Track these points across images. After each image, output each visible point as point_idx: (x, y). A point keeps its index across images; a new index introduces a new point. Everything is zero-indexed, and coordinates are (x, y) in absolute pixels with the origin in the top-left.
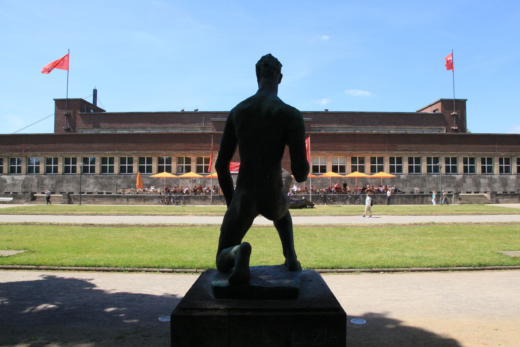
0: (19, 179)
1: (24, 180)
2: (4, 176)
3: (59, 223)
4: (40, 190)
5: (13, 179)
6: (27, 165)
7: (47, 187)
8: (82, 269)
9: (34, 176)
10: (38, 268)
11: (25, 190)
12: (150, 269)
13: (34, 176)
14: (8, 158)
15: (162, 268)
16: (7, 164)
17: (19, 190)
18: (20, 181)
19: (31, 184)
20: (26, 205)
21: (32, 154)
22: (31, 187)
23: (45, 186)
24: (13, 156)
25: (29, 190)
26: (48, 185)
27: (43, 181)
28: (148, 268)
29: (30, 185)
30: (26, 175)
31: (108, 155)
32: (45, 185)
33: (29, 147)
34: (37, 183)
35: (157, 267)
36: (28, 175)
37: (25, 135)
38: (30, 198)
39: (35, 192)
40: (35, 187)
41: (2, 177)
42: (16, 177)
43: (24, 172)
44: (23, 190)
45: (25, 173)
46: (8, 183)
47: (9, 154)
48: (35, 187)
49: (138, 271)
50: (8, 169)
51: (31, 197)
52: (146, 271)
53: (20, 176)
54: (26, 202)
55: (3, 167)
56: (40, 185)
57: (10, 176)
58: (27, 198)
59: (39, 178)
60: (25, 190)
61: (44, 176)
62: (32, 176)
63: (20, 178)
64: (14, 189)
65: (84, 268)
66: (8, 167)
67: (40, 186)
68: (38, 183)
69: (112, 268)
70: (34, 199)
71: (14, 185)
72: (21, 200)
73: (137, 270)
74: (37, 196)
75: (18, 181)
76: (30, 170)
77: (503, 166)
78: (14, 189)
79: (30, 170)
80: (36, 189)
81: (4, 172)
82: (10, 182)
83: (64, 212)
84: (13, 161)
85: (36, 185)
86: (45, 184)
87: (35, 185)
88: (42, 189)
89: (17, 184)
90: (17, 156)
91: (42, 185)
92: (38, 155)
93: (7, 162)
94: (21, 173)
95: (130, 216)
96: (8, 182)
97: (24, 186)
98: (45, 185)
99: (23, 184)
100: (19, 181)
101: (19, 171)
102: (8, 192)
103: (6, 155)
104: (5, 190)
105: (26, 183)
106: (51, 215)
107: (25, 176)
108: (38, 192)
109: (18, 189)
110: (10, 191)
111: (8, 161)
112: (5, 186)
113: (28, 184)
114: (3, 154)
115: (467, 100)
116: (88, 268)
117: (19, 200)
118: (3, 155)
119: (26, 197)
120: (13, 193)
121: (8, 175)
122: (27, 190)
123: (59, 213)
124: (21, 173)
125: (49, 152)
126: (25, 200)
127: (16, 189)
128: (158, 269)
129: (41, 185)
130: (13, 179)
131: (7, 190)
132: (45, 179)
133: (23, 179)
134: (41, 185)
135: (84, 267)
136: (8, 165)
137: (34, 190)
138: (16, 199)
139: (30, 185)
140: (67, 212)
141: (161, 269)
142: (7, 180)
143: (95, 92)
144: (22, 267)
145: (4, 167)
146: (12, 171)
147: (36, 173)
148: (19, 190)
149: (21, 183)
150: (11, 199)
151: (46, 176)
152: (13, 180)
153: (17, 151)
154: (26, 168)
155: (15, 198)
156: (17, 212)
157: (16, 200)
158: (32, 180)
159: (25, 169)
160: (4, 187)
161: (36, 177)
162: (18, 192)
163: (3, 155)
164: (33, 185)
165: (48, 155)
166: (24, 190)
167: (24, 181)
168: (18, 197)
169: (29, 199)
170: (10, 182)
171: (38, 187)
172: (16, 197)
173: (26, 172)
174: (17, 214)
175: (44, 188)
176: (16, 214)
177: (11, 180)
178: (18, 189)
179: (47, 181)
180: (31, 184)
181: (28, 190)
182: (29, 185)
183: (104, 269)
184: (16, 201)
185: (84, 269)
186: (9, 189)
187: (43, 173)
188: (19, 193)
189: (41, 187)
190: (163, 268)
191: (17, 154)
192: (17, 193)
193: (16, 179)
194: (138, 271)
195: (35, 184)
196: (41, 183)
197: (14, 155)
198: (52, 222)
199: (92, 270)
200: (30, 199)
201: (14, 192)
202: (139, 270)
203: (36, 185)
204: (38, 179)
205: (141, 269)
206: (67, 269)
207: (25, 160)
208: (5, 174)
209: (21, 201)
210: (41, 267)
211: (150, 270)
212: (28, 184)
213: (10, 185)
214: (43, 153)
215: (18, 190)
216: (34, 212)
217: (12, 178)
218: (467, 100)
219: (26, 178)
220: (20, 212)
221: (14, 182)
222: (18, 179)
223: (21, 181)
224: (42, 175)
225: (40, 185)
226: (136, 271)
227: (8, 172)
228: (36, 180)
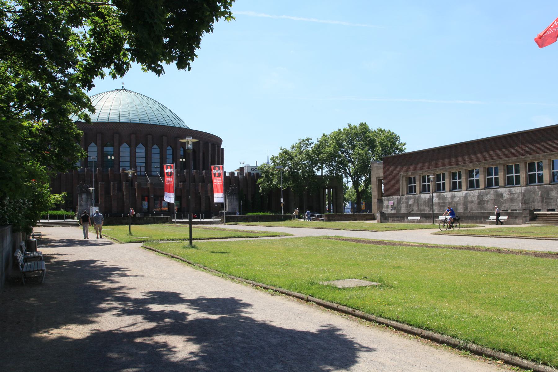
0: (518, 192)
1: (523, 193)
2: (500, 189)
3: (510, 250)
4: (545, 206)
5: (511, 193)
6: (526, 172)
7: (554, 201)
8: (403, 328)
9: (536, 187)
10: (354, 312)
11: (526, 206)
12: (517, 359)
13: (536, 186)
14: (504, 165)
15: (543, 364)
16: (502, 173)
17: (518, 206)
18: (519, 194)
19: (534, 198)
20: (523, 226)
21: (532, 157)
22: (533, 202)
23: (552, 201)
24: (509, 163)
25: (531, 206)
26: (555, 198)
27: (548, 194)
28: (512, 354)
29: (531, 200)
30: (526, 186)
31: (471, 167)
32: (551, 199)
33: (528, 148)
34: (541, 196)
35: (533, 357)
36: (528, 186)
37: (521, 133)
38: (528, 217)
39: (539, 208)
40: (538, 202)
41: (498, 191)
42: (513, 190)
43: (523, 182)
44: (523, 206)
45: (525, 183)
46: (505, 198)
47: (504, 160)
48: (538, 202)
49: (490, 356)
50: (505, 180)
51: (530, 215)
52: (507, 362)
53: (519, 188)
54: (524, 222)
55: (498, 177)
56: (545, 198)
57: (506, 189)
58: (525, 217)
59: (543, 190)
60: (526, 206)
61: (550, 186)
62: (534, 187)
63: (519, 190)
64: (512, 205)
65: (406, 327)
66: (504, 177)
67: (545, 201)
68: (541, 196)
69: (445, 338)
70: (533, 218)
71: (512, 200)
72: (517, 220)
73: (489, 353)
74: (538, 214)
75: (516, 195)
76: (531, 180)
77: (515, 173)
78: (512, 205)
79: (531, 180)
80: (540, 204)
81: (499, 185)
82: (508, 196)
83: (551, 236)
84: (509, 170)
85: (539, 199)
86: (552, 197)
87: (538, 199)
88: (548, 205)
89: (515, 200)
90: (513, 162)
91: (548, 198)
92: (540, 158)
93: (502, 170)
94: (519, 184)
95: (456, 236)
96: (505, 196)
97: (525, 201)
98: (551, 199)
99: (523, 198)
100: (518, 195)
101: (518, 182)
102: (505, 209)
103: (501, 162)
104: (502, 207)
105: (527, 197)
106: (531, 239)
107: (525, 187)
108: (543, 209)
109: (518, 205)
110: (507, 208)
111: (504, 170)
112: (502, 201)
113: (529, 198)
114: (497, 161)
116: (411, 327)
117: (515, 220)
118: (498, 162)
119: (523, 216)
120: (512, 210)
121: (504, 188)
122: (528, 206)
123: (543, 236)
124: (519, 184)
125: (554, 152)
126: (522, 219)
127: (514, 205)
128: (533, 363)
129: (546, 199)
130: (511, 193)
131: (505, 206)
132: (551, 190)
133: (523, 191)
134: (546, 199)
135: (406, 326)
136: (504, 174)
137: (537, 206)
138: (512, 219)
139: (531, 200)
140: (554, 236)
141: (540, 366)
142: (504, 195)
143: (256, 161)
144: (341, 307)
145: (499, 178)
146: (509, 182)
147: (539, 182)
148: (518, 206)
149: (521, 197)
150: (419, 218)
151: (552, 185)
152: (511, 194)
153: (513, 155)
154: (526, 177)
155: (510, 218)
156: (488, 234)
157: (511, 220)
158: (534, 192)
159: (524, 179)
160: (500, 203)
161: (539, 188)
162: (518, 209)
163: (498, 162)
164: (536, 199)
165: (553, 156)
166: (525, 206)
167: (524, 194)
168: (514, 216)
169: (527, 218)
170: (508, 196)
171: (542, 202)
172: (512, 216)
173: (526, 182)
174: (488, 237)
175: (551, 202)
176: (487, 236)
177: (509, 194)
178: (518, 205)
179: (554, 192)
180: (534, 198)
181: (529, 207)
182: (531, 199)
183: (433, 336)
184: (512, 220)
185: (406, 328)
186: (506, 206)
187: (548, 182)
188: (519, 210)
189: (546, 202)
190: (547, 365)
191: (513, 159)
192: (516, 210)
193: (514, 192)
194: (490, 356)
195: (538, 198)
196: (546, 196)
197: (510, 161)
198: (471, 244)
199: (415, 334)
200: (528, 218)
201: (513, 209)
202: (492, 354)
203: (539, 199)
204: (542, 191)
205: (497, 355)
206: (385, 322)
207: (524, 166)
208: (501, 187)
209: (517, 221)
210: (357, 311)
211: (516, 362)
212: (529, 198)
213: (507, 200)
214: (546, 154)
215: (517, 207)
216: (509, 235)
217: (509, 192)
219: (525, 191)
220: (492, 234)
221: (512, 196)
222: (516, 192)
223: (520, 195)
224: (546, 185)
225: (545, 198)
226: (487, 356)
227: (505, 183)
228: (540, 192)
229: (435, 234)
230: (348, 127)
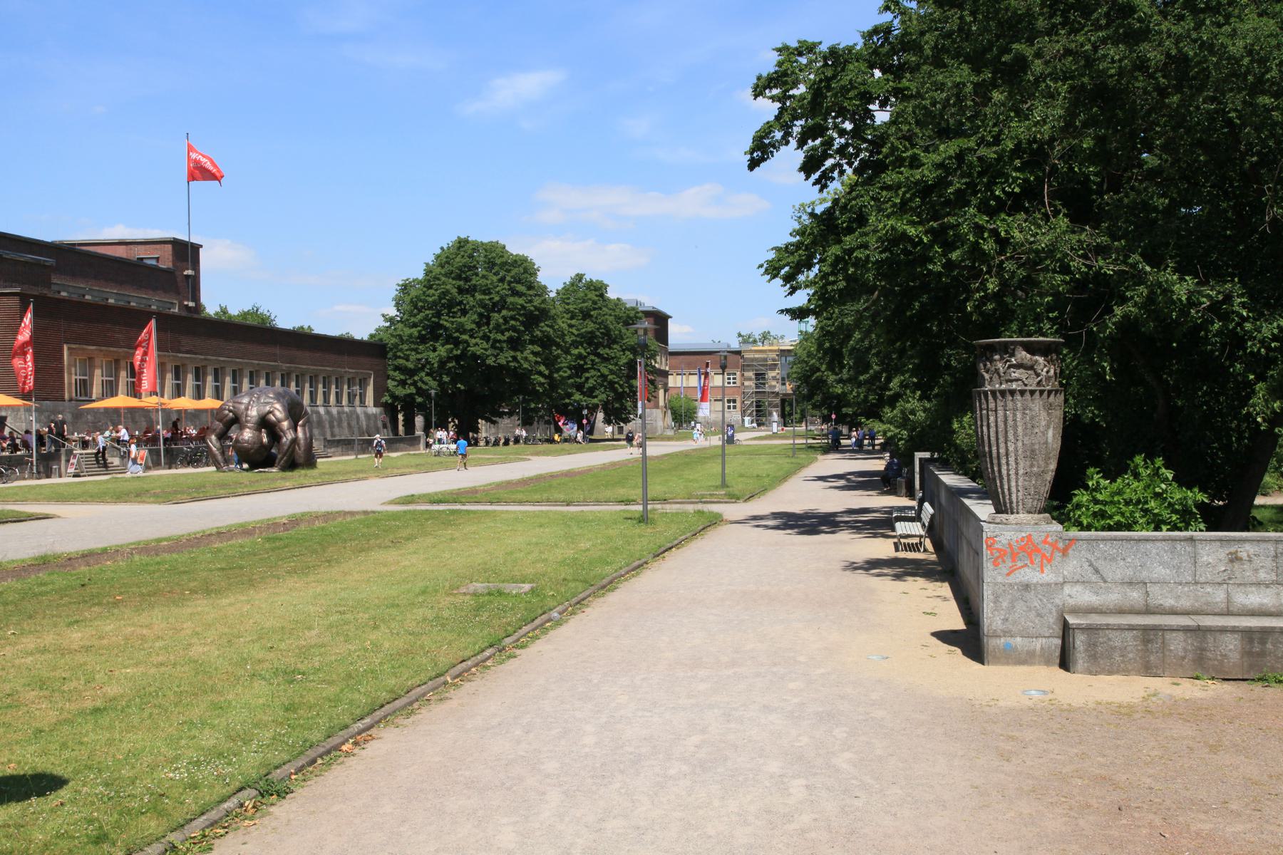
218: (201, 246)
229: (873, 565)
230: (219, 310)
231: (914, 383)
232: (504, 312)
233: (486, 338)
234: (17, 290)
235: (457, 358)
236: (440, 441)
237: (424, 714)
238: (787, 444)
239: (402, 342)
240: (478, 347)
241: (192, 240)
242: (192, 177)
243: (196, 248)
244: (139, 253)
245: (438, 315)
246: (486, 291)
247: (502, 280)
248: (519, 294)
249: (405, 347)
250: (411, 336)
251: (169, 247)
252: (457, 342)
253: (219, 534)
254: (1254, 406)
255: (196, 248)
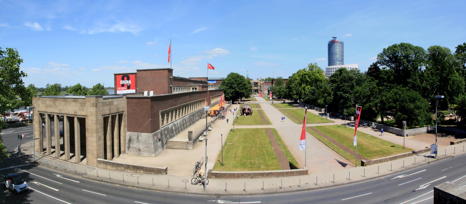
115: (173, 69)
218: (173, 69)
231: (430, 104)
232: (241, 84)
233: (239, 88)
234: (201, 85)
235: (234, 91)
236: (413, 55)
237: (291, 177)
238: (332, 66)
239: (227, 89)
240: (238, 90)
241: (172, 68)
242: (209, 68)
243: (172, 70)
244: (202, 79)
245: (231, 85)
246: (238, 81)
247: (240, 79)
248: (243, 82)
249: (227, 90)
250: (228, 88)
251: (167, 71)
252: (234, 89)
253: (247, 125)
254: (425, 85)
255: (172, 70)
